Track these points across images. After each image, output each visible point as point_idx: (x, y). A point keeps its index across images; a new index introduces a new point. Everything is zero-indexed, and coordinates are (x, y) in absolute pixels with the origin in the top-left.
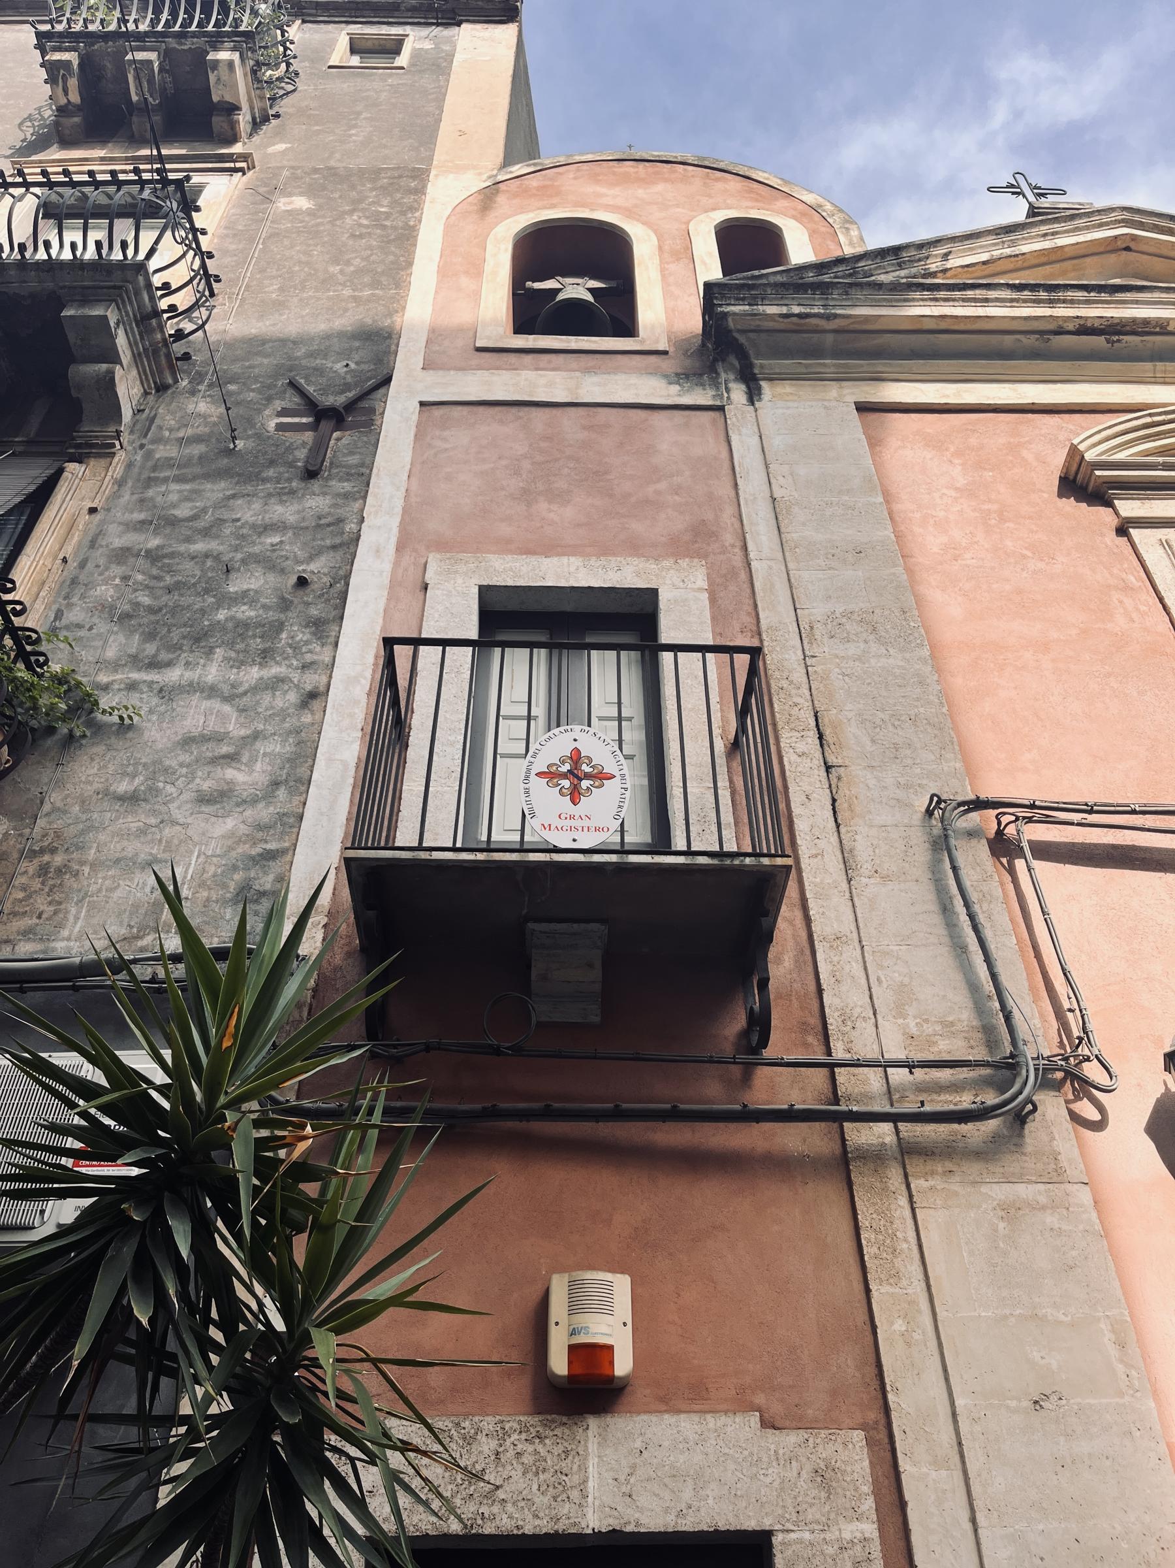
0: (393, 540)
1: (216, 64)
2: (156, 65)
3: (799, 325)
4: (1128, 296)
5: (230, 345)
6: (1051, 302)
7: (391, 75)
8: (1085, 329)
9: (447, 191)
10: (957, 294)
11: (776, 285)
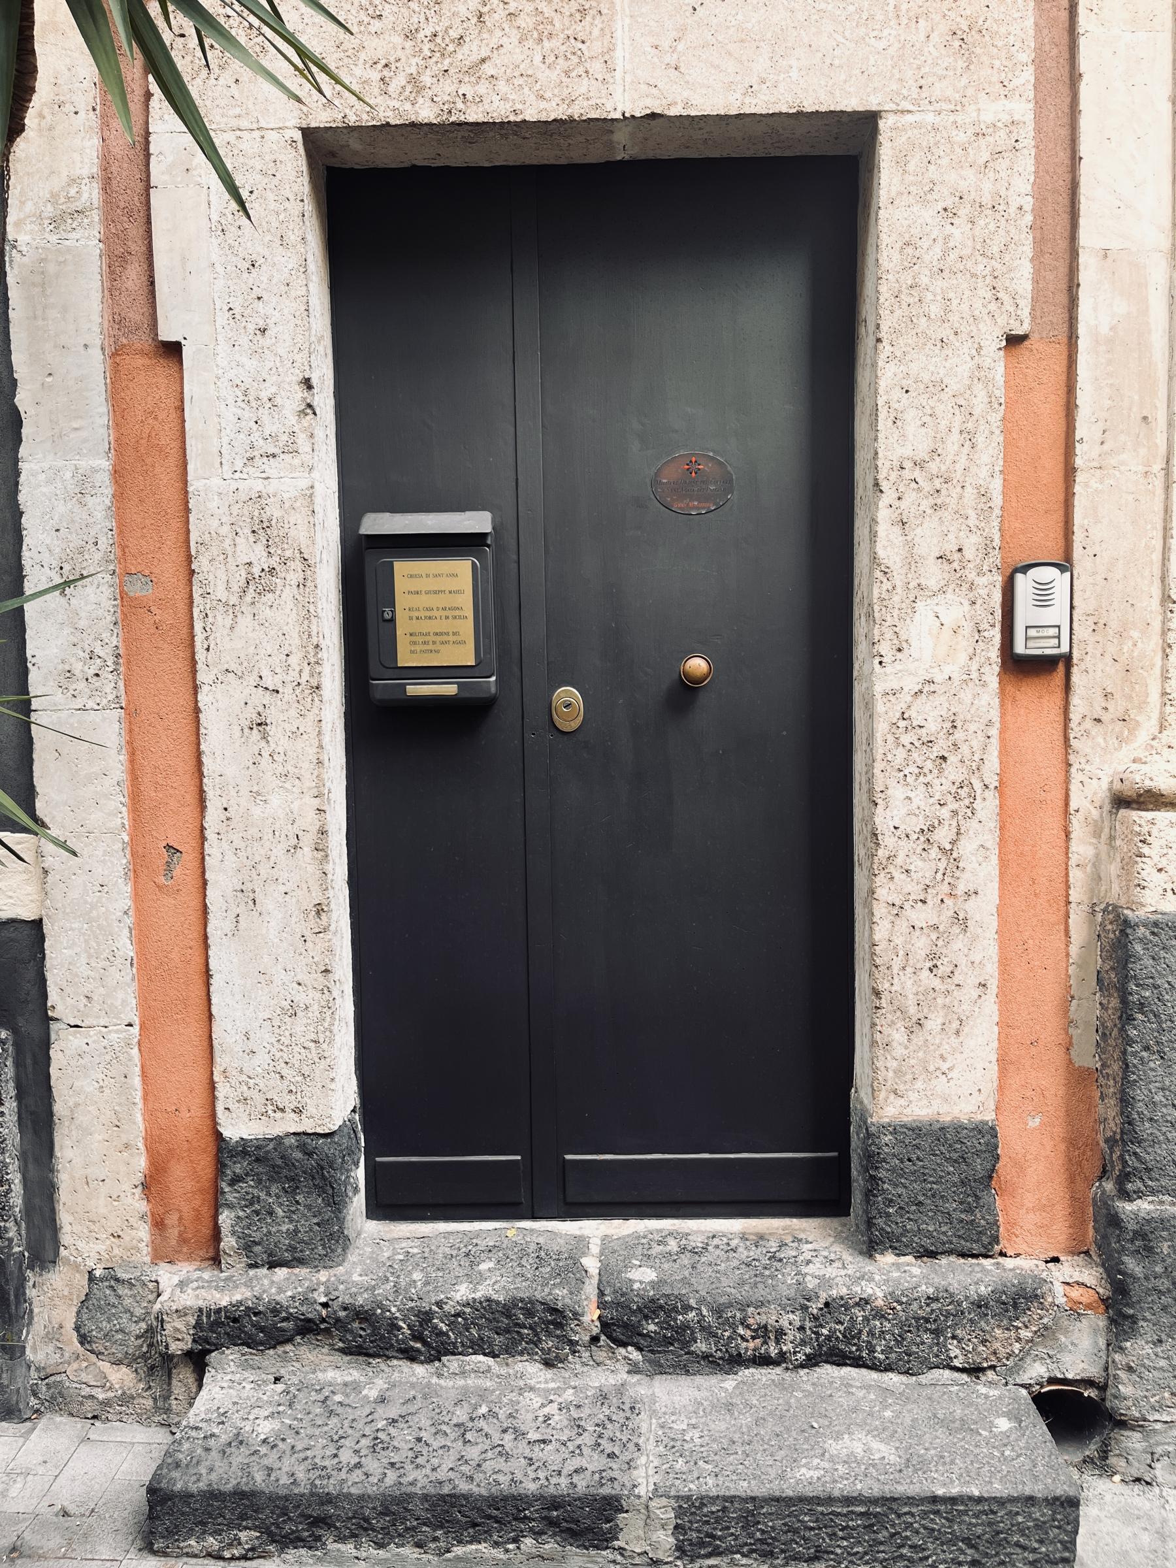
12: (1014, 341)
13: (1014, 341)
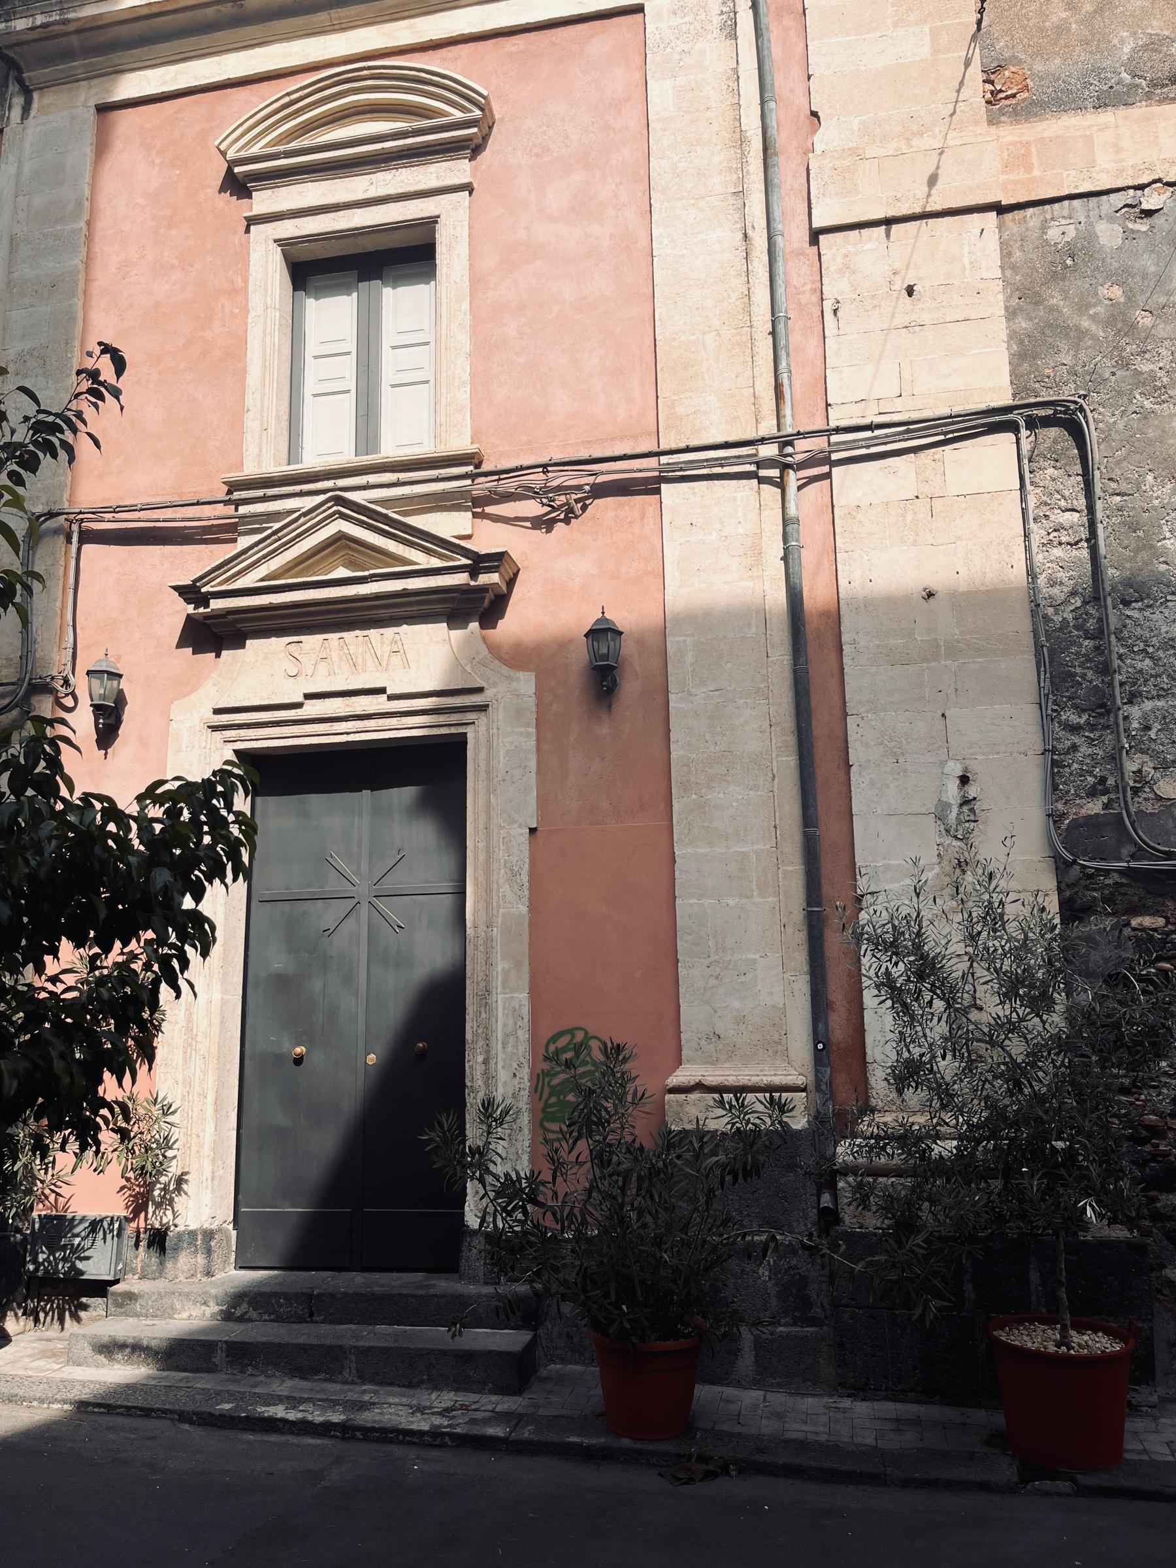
12: (533, 831)
13: (533, 831)
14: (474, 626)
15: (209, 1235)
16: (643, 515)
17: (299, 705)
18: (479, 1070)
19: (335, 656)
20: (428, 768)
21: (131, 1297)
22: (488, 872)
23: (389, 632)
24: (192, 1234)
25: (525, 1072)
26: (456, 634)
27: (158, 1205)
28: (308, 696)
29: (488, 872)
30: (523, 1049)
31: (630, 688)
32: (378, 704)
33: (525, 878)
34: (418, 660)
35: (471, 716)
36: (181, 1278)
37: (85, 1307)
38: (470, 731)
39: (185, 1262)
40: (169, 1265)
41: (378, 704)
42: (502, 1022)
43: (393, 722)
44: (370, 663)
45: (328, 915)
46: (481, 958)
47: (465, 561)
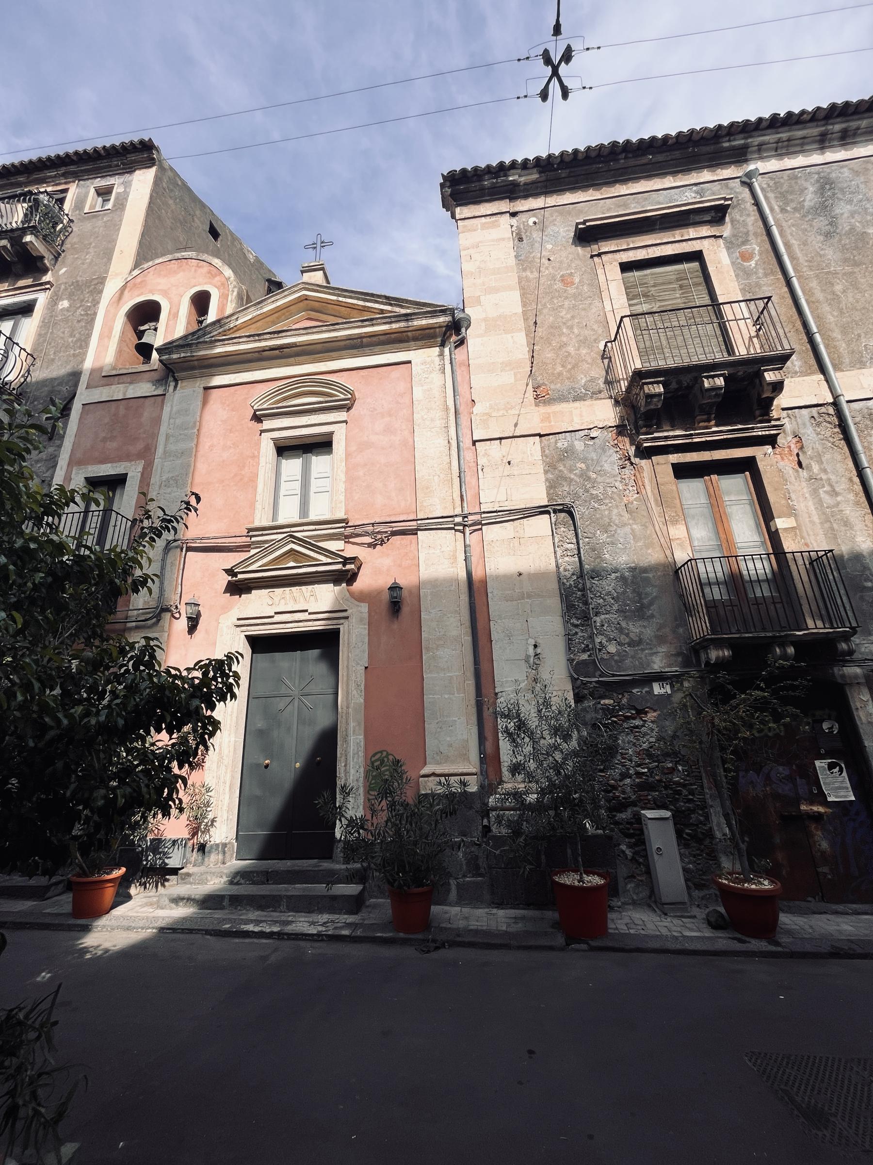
0: (67, 463)
1: (26, 243)
2: (9, 246)
3: (185, 360)
4: (284, 334)
5: (37, 383)
6: (260, 340)
7: (105, 215)
8: (272, 349)
9: (111, 288)
10: (231, 341)
11: (176, 346)
12: (366, 668)
13: (366, 668)
14: (344, 585)
15: (225, 845)
16: (411, 543)
17: (272, 617)
18: (343, 769)
19: (288, 596)
20: (324, 642)
21: (188, 875)
22: (348, 685)
23: (310, 587)
24: (217, 845)
25: (362, 770)
26: (337, 588)
27: (203, 832)
28: (276, 613)
29: (348, 685)
30: (361, 760)
31: (406, 610)
32: (305, 616)
33: (363, 687)
34: (322, 598)
35: (342, 621)
36: (211, 865)
37: (168, 880)
38: (341, 627)
39: (213, 858)
40: (206, 859)
41: (305, 616)
42: (352, 748)
43: (310, 623)
44: (302, 599)
45: (281, 704)
46: (344, 721)
47: (341, 560)
